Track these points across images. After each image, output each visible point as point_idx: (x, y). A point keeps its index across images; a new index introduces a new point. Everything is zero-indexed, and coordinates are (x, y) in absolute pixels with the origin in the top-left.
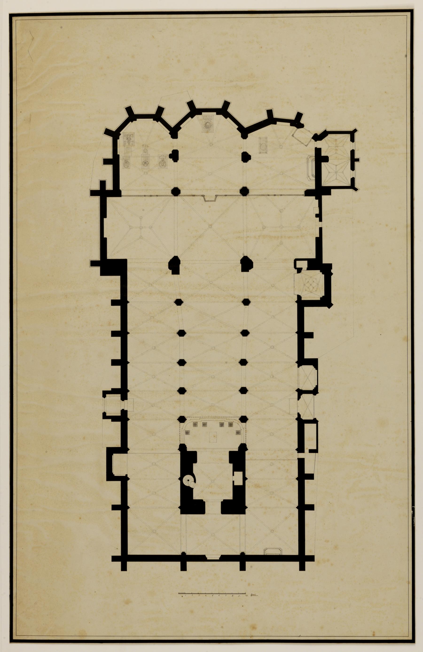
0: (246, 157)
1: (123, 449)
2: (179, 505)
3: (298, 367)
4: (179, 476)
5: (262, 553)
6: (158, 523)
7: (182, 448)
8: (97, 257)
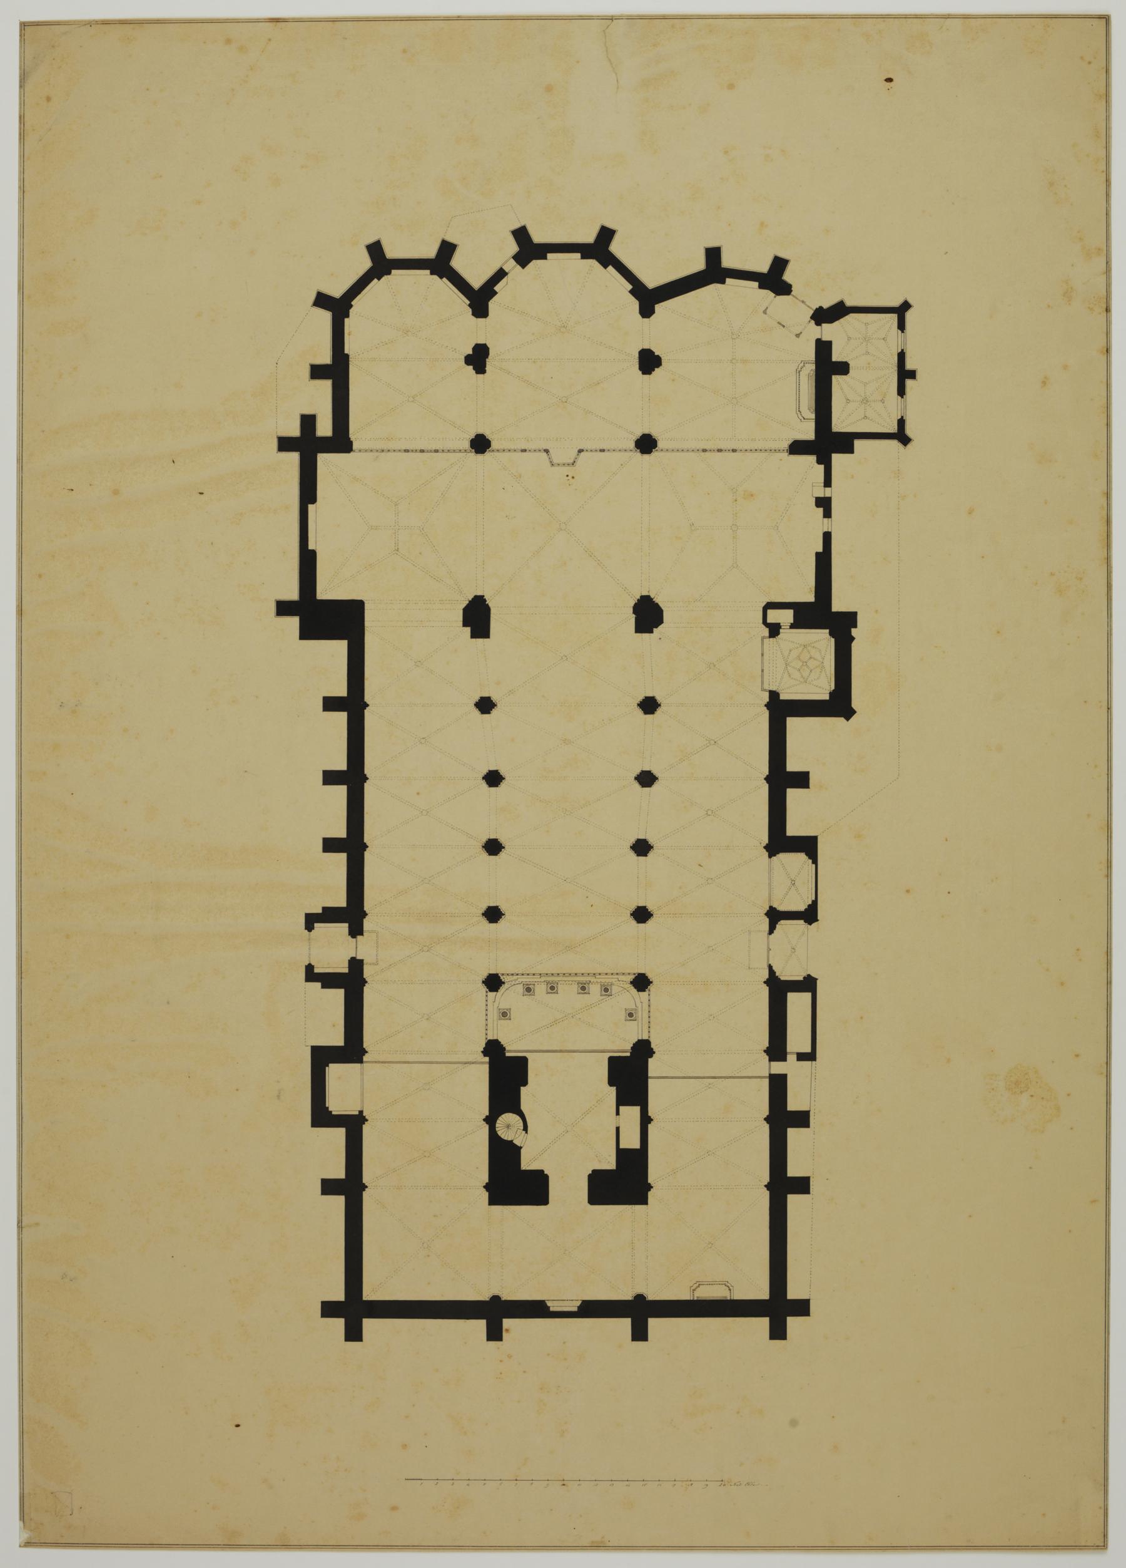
0: (649, 362)
1: (352, 1050)
2: (485, 1179)
3: (770, 857)
4: (486, 1112)
5: (685, 1295)
6: (435, 1224)
7: (493, 1049)
8: (292, 593)
